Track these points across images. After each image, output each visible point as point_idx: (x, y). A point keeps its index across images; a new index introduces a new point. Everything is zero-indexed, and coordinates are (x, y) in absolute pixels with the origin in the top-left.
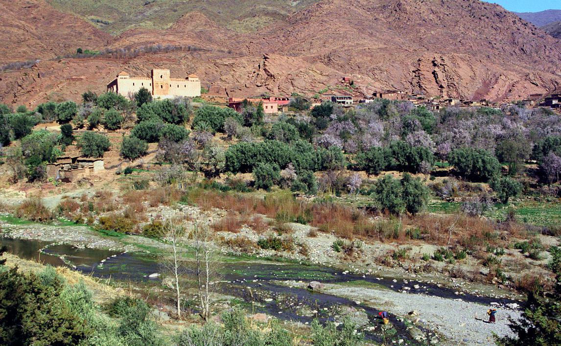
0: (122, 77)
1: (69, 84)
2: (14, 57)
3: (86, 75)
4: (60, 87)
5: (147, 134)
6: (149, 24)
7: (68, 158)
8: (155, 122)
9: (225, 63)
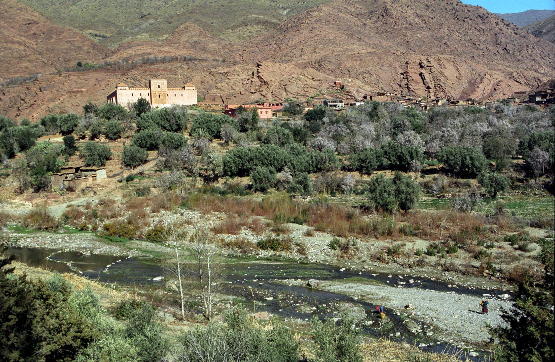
0: (121, 88)
1: (70, 97)
6: (146, 36)
7: (71, 168)
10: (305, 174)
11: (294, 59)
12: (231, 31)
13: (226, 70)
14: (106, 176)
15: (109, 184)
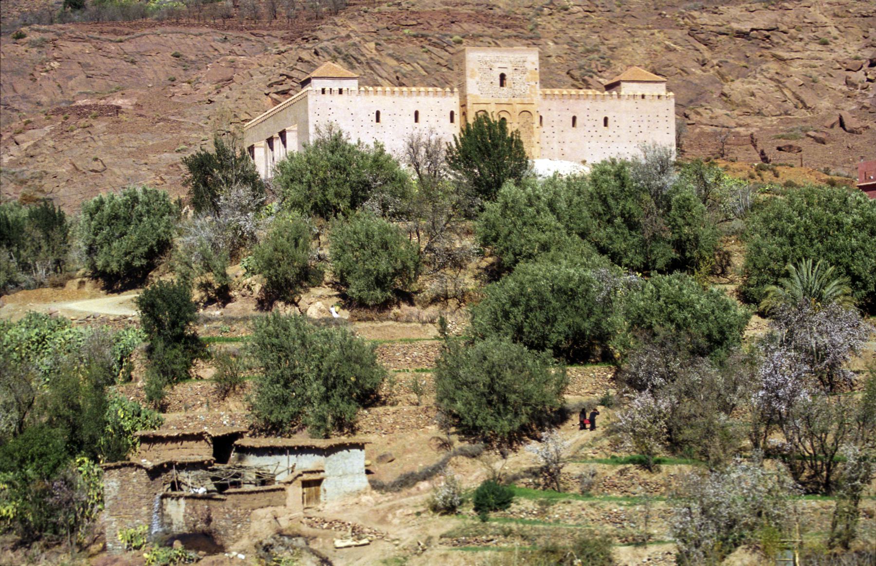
0: (328, 84)
1: (63, 133)
3: (128, 91)
5: (550, 321)
7: (199, 437)
8: (572, 265)
9: (735, 26)
13: (763, 19)
14: (363, 481)
15: (383, 520)
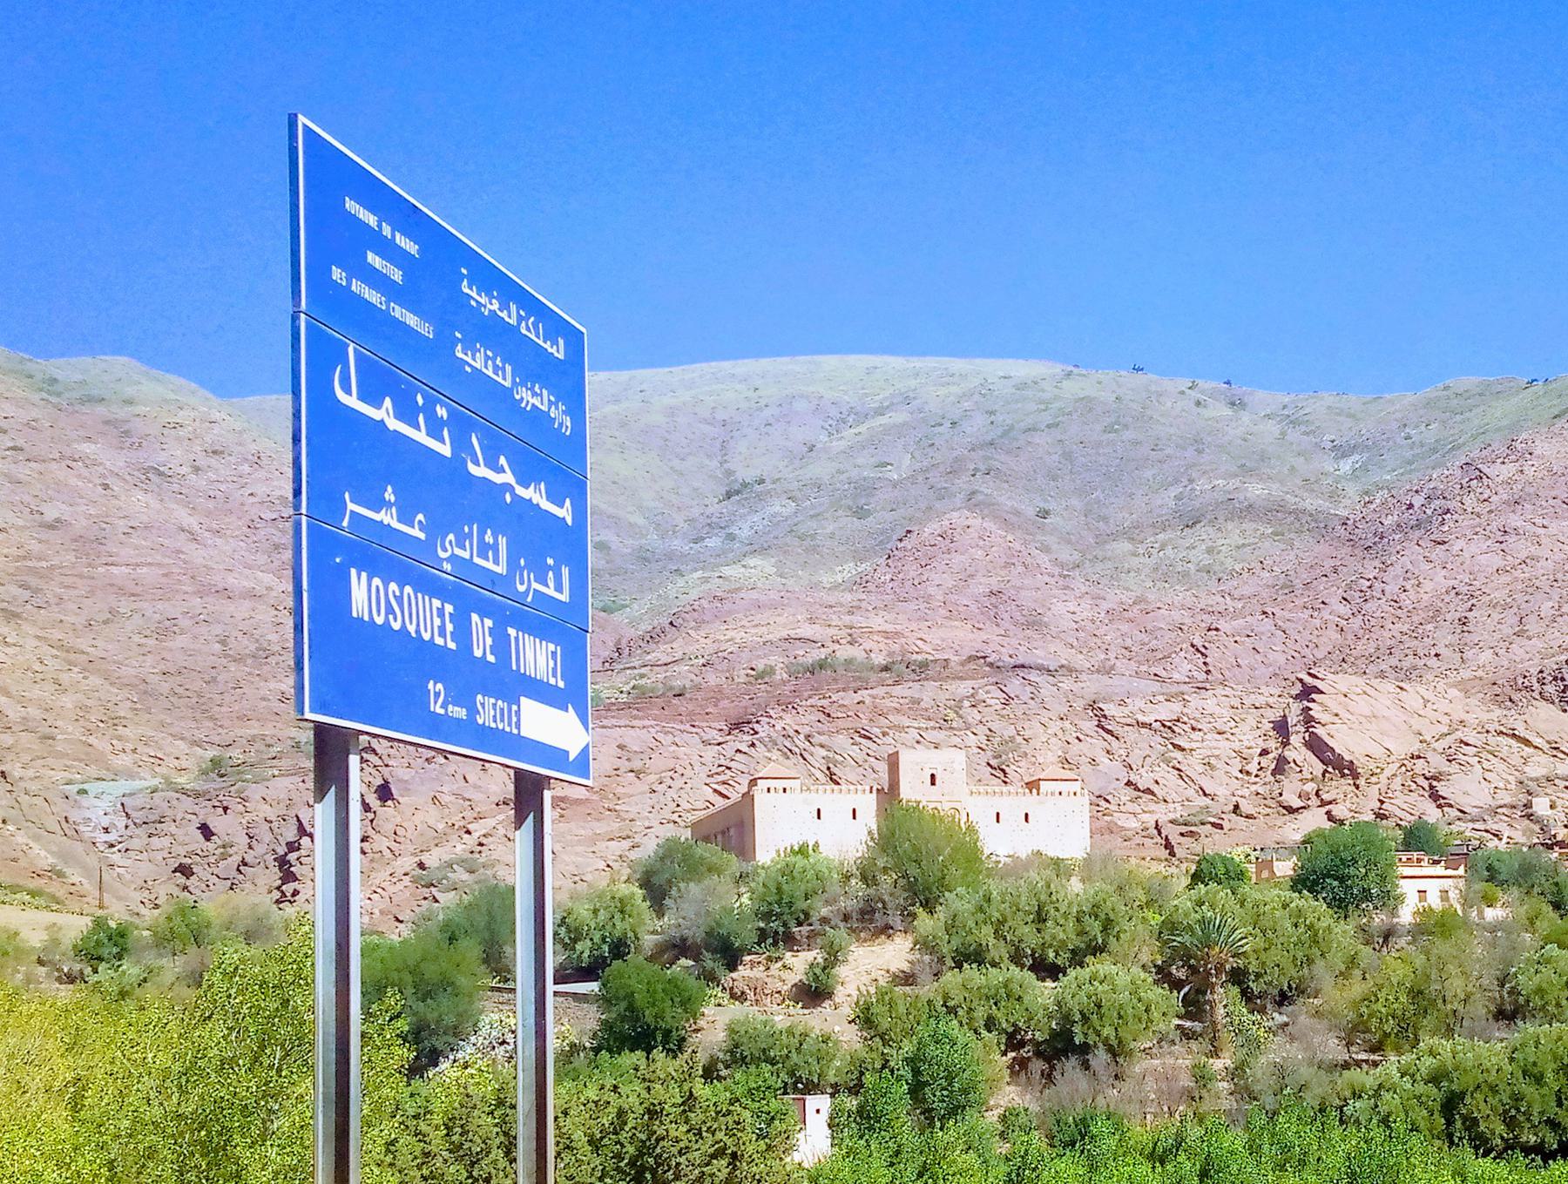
2: (244, 718)
4: (475, 835)
6: (761, 566)
10: (1243, 1122)
11: (1433, 662)
12: (1126, 546)
